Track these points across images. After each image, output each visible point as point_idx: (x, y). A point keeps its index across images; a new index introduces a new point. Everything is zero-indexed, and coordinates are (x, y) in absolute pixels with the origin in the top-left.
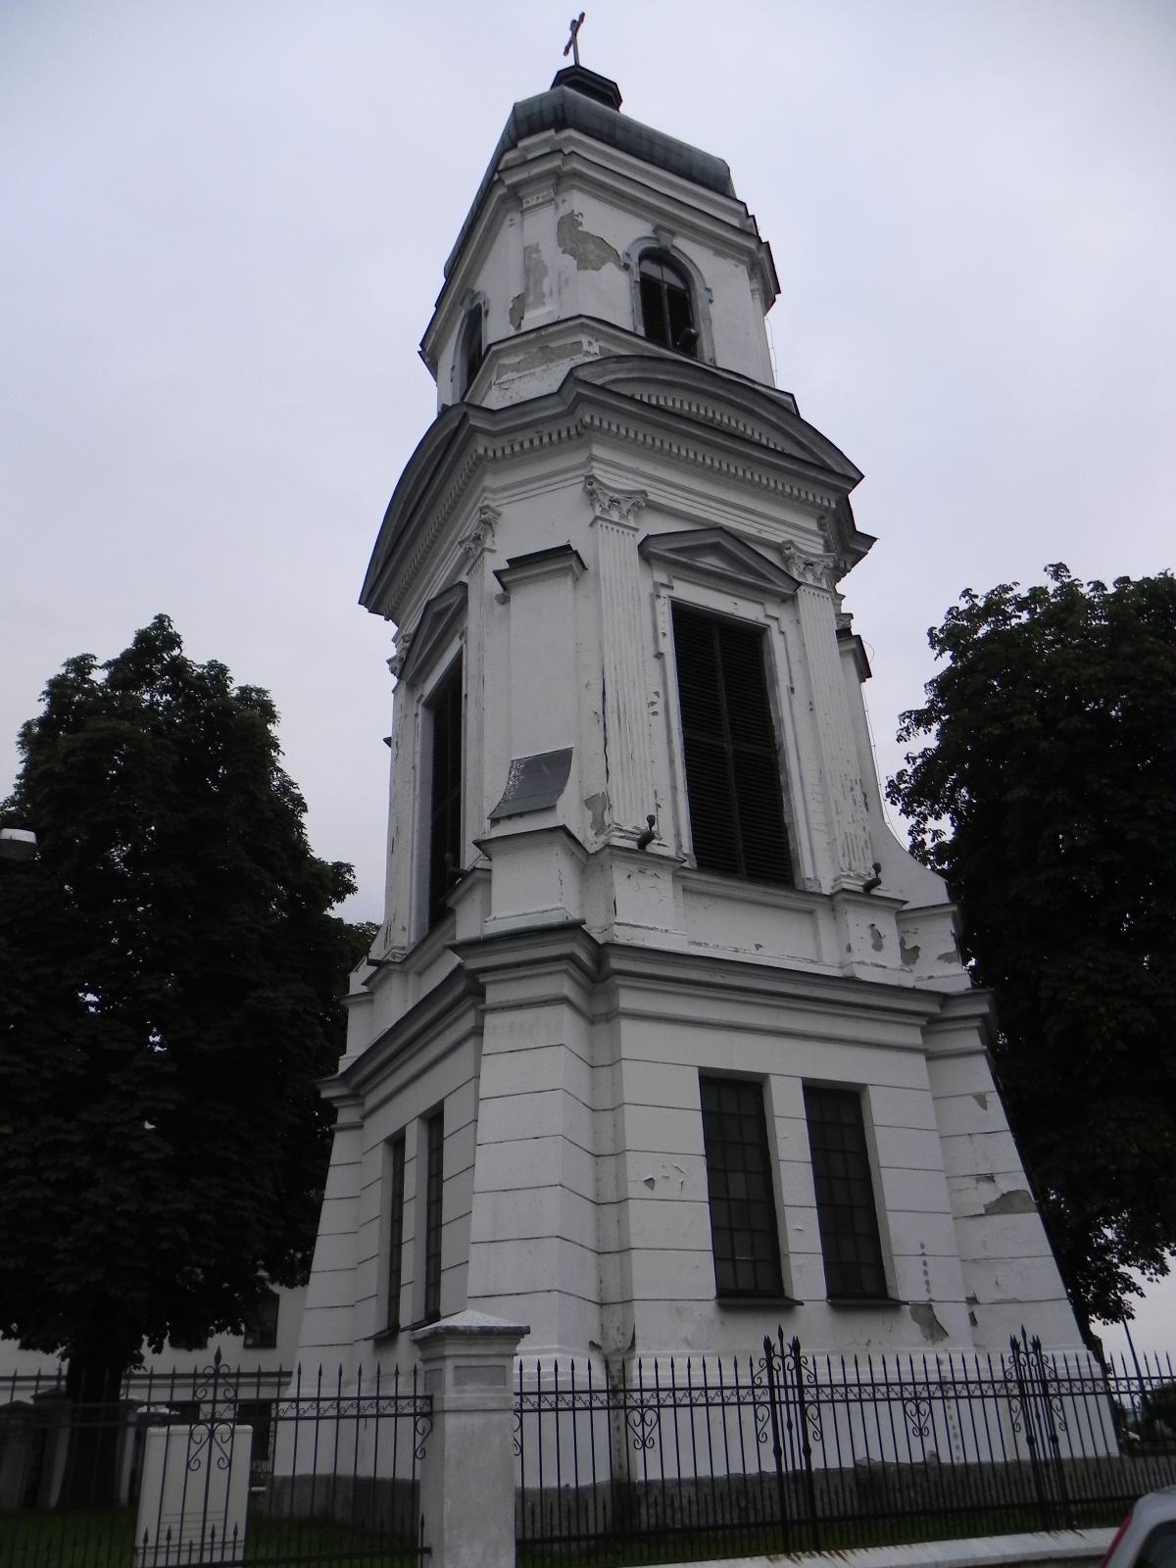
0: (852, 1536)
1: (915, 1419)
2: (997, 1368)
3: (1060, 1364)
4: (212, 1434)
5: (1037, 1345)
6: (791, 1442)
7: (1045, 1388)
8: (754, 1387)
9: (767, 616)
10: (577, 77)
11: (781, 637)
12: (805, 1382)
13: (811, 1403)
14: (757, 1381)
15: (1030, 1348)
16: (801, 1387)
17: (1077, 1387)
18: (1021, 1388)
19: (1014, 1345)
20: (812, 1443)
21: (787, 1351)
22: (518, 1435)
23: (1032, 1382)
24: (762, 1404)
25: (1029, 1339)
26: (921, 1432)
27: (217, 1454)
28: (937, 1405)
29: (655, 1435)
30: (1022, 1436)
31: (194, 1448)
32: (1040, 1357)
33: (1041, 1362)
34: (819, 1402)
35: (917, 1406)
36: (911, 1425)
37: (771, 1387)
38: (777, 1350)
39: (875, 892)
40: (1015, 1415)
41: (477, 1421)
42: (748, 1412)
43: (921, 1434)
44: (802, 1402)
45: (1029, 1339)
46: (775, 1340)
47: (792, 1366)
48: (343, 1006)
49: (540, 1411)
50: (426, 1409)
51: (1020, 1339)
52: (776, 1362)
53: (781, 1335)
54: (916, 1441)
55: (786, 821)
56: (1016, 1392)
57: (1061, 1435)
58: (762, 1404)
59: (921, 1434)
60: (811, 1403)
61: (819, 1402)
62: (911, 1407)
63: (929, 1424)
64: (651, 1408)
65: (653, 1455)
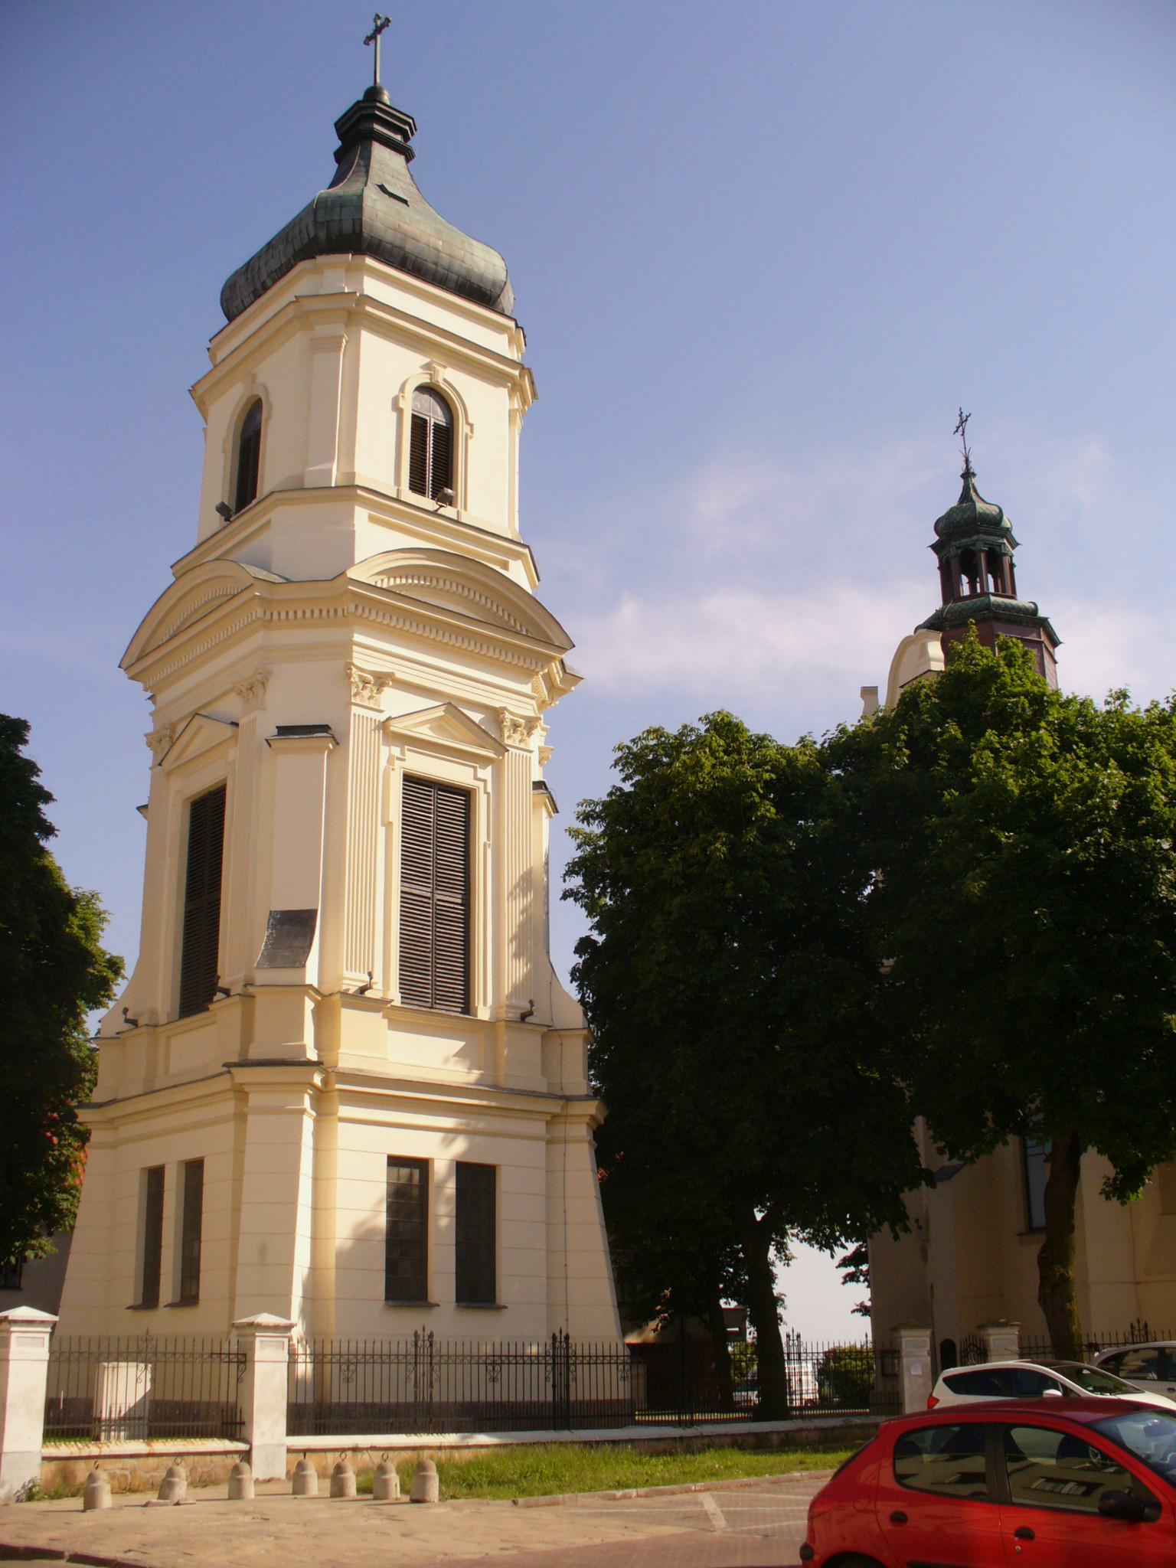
1: (346, 1373)
3: (579, 1348)
5: (798, 1336)
7: (800, 1357)
9: (476, 778)
10: (408, 128)
11: (486, 796)
12: (434, 1354)
14: (141, 1349)
15: (795, 1338)
16: (568, 1357)
21: (563, 1339)
23: (424, 1356)
25: (795, 1334)
26: (494, 1380)
28: (505, 1367)
29: (354, 1376)
30: (550, 1384)
31: (139, 1373)
32: (799, 1342)
33: (799, 1346)
35: (348, 1367)
38: (558, 1339)
39: (528, 1019)
41: (271, 1366)
43: (348, 1381)
45: (795, 1334)
48: (876, 1228)
49: (617, 1356)
50: (243, 1360)
53: (424, 1329)
56: (551, 1361)
59: (348, 1381)
62: (490, 1368)
64: (353, 1363)
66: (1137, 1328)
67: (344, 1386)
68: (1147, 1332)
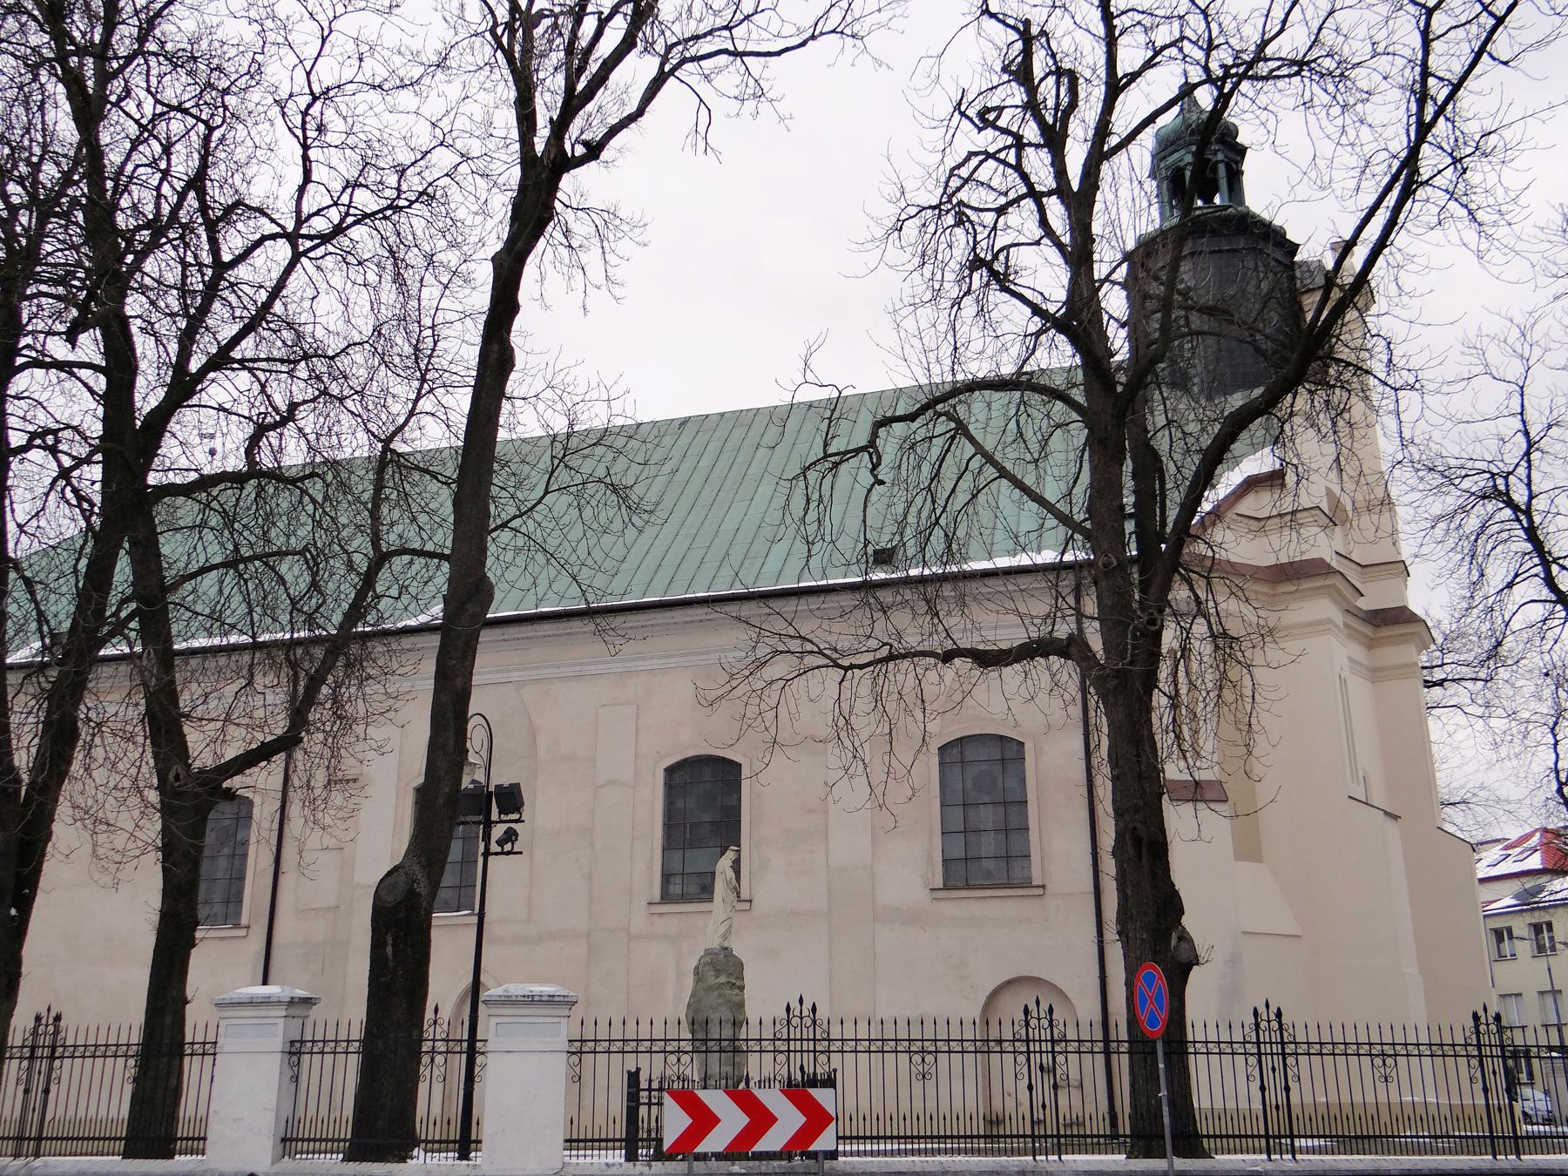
0: (1348, 1147)
1: (1382, 1070)
2: (1085, 1029)
4: (432, 1061)
6: (1274, 1082)
8: (1466, 1045)
13: (1060, 1053)
17: (1327, 1049)
18: (1480, 1050)
19: (1476, 1017)
20: (1291, 1083)
21: (1273, 1017)
22: (577, 1069)
24: (1021, 1053)
25: (1273, 1009)
27: (436, 1072)
34: (1297, 1054)
36: (1377, 1074)
37: (1258, 1043)
38: (1035, 1014)
40: (1472, 1071)
42: (1009, 1058)
44: (1284, 1054)
46: (1032, 1007)
47: (1495, 1031)
51: (1481, 1013)
52: (1483, 1028)
53: (1038, 1003)
54: (1381, 1087)
55: (1217, 472)
57: (1293, 1085)
58: (1021, 1053)
60: (1060, 1053)
61: (1297, 1054)
62: (1378, 1061)
63: (1394, 1074)
65: (1393, 1086)
66: (1265, 1017)
67: (917, 1085)
68: (814, 1022)
